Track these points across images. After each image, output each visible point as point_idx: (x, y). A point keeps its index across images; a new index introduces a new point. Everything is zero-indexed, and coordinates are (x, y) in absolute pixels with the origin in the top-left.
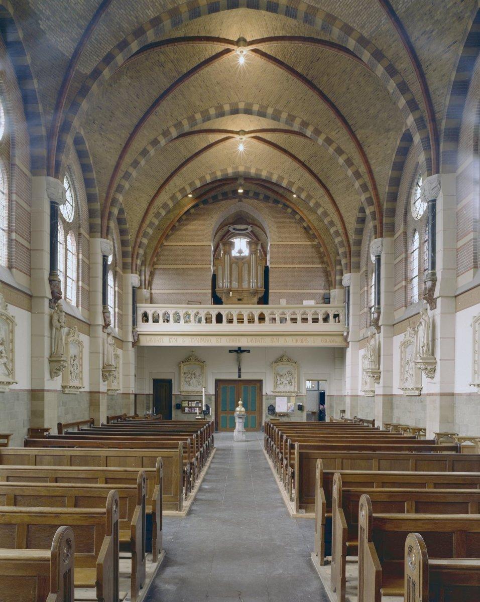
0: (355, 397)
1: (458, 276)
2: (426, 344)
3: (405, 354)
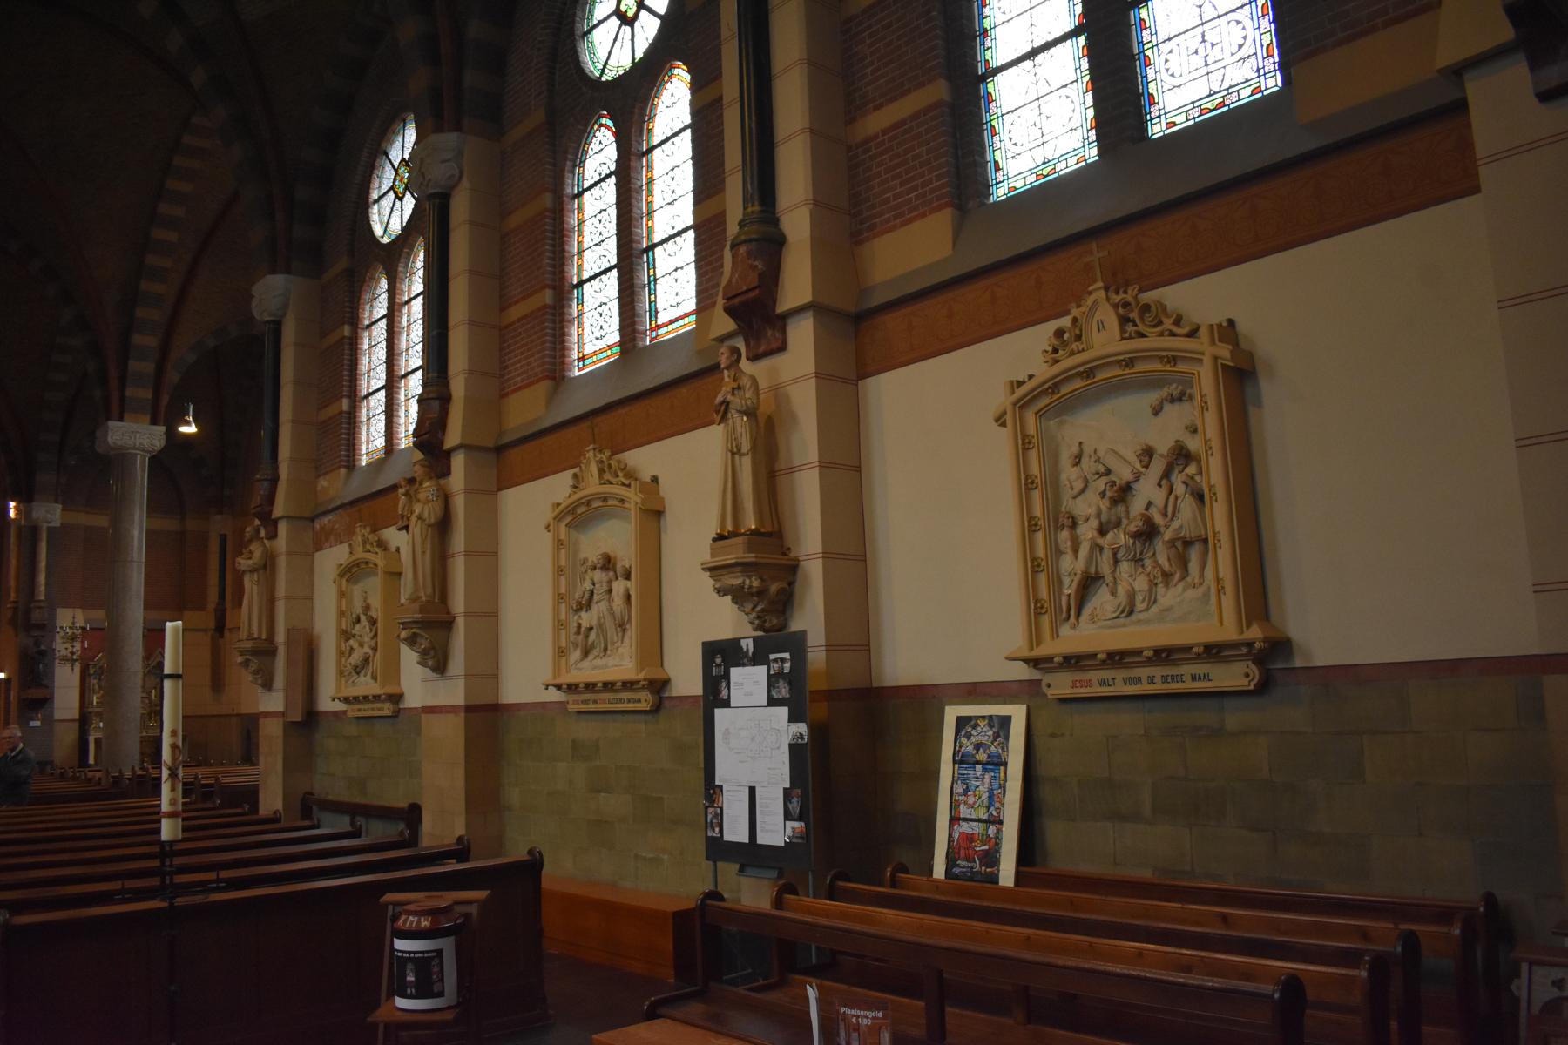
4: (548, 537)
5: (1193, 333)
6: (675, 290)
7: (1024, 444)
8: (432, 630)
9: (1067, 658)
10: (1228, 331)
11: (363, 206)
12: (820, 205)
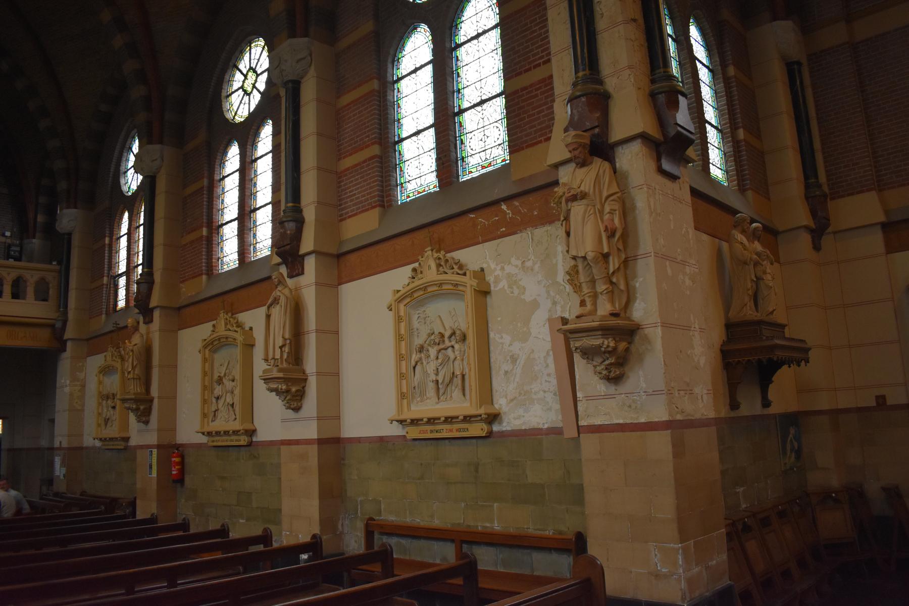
0: (76, 453)
1: (341, 220)
2: (288, 342)
3: (213, 362)
4: (199, 357)
5: (465, 274)
6: (486, 140)
7: (399, 319)
8: (142, 407)
9: (412, 421)
10: (481, 274)
11: (118, 173)
12: (320, 203)
